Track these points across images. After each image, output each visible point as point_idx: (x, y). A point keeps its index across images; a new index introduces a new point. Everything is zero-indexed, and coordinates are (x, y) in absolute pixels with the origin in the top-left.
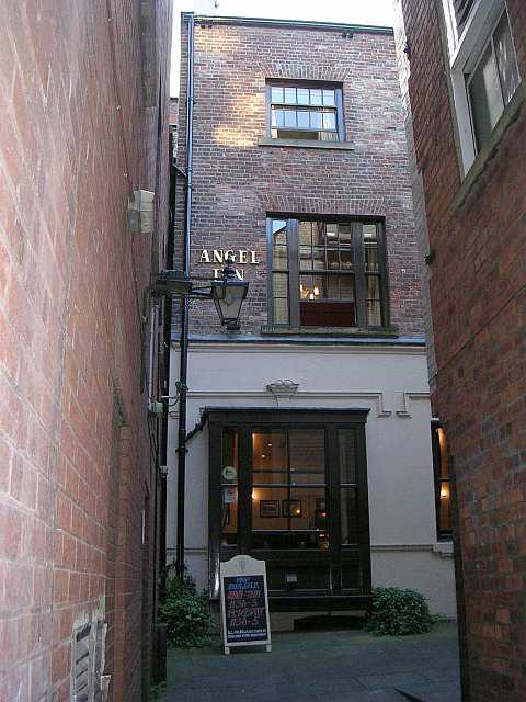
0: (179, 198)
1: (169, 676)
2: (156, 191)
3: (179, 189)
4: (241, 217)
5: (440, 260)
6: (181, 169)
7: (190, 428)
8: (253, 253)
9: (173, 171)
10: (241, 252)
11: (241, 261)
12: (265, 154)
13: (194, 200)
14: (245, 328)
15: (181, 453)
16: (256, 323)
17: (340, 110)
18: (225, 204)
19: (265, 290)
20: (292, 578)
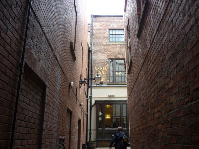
0: (90, 56)
3: (90, 54)
6: (91, 50)
8: (106, 67)
10: (103, 67)
11: (103, 69)
14: (104, 83)
15: (91, 110)
16: (106, 82)
18: (100, 57)
19: (108, 76)
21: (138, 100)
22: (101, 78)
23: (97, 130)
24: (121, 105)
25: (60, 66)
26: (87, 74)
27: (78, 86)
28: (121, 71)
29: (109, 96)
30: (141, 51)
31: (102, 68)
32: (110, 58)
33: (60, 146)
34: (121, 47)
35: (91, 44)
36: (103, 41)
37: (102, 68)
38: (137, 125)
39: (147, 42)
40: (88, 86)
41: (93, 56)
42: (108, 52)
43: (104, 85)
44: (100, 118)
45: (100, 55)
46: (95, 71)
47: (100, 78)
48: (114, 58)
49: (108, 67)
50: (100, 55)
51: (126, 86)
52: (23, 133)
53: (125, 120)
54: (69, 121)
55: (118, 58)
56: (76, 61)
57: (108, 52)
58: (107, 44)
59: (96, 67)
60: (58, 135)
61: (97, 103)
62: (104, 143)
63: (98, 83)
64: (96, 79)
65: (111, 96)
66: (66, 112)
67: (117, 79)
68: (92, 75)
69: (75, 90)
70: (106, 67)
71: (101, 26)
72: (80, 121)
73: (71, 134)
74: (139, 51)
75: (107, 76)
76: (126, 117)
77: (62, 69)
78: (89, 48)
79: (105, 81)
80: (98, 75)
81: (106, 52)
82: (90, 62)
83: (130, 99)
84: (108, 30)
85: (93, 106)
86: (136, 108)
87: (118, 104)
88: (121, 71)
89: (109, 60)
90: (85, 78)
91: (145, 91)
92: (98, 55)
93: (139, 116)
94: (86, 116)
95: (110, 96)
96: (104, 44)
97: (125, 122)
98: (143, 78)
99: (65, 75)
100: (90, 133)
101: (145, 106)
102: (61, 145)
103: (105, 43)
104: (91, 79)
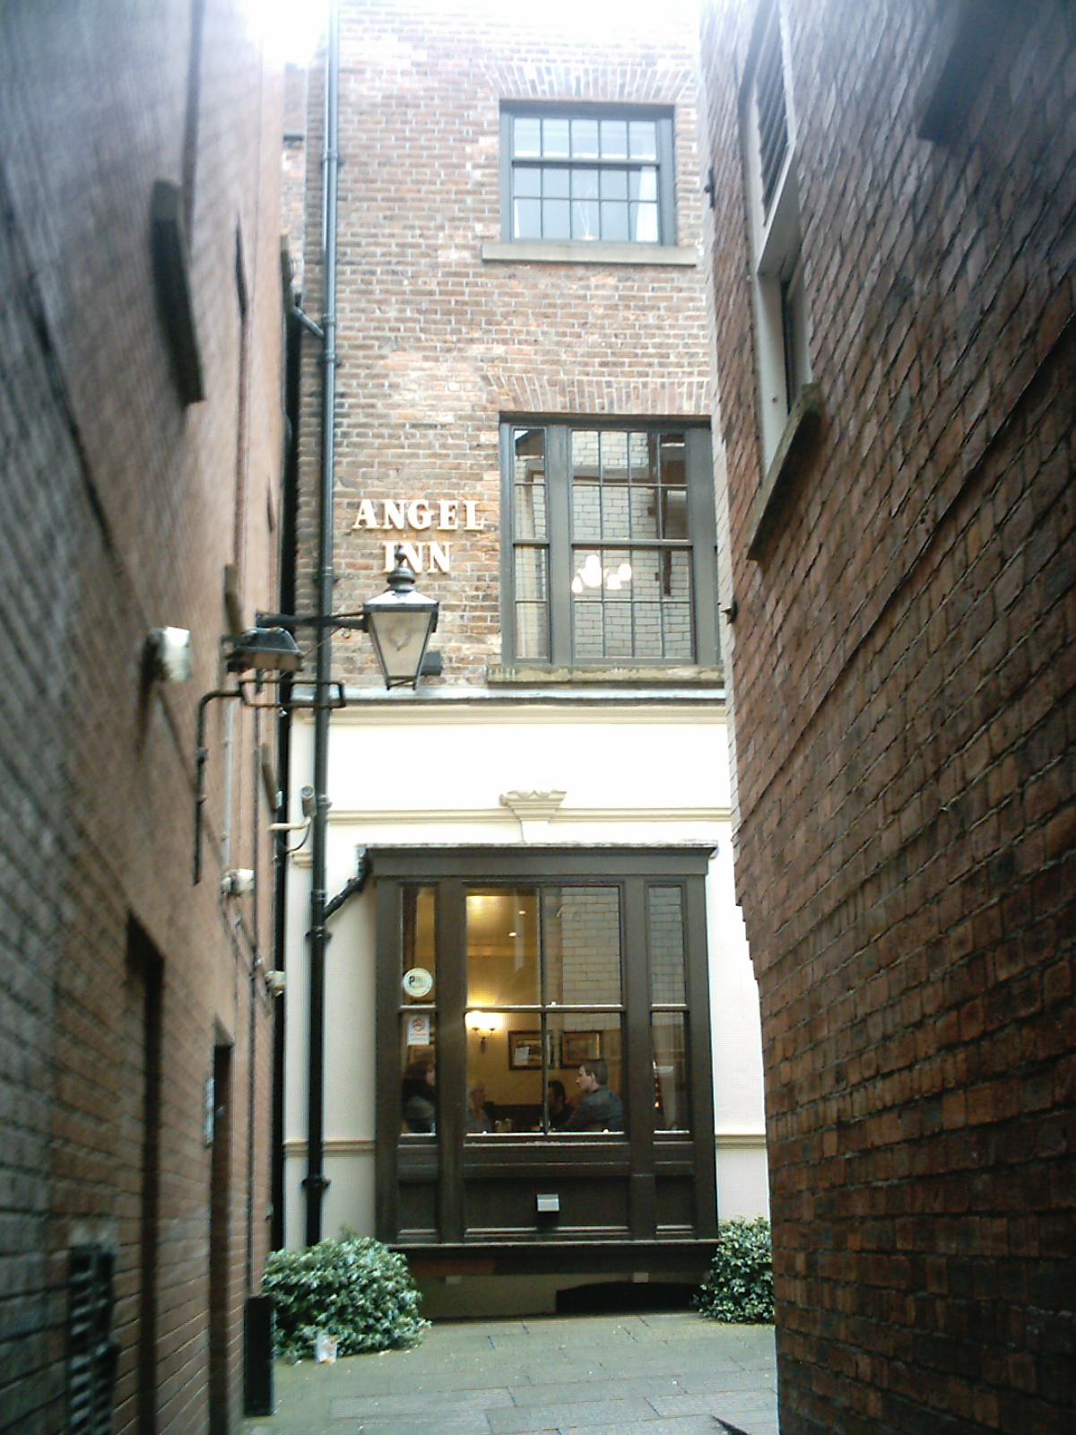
0: (308, 385)
1: (279, 1399)
2: (255, 868)
3: (307, 365)
4: (443, 426)
5: (742, 615)
6: (311, 319)
7: (335, 885)
8: (471, 505)
9: (295, 333)
10: (445, 504)
11: (445, 525)
12: (493, 281)
13: (341, 389)
14: (454, 670)
15: (317, 943)
16: (477, 660)
17: (666, 169)
18: (409, 396)
19: (497, 590)
20: (549, 1203)
21: (910, 820)
22: (433, 612)
23: (383, 1146)
24: (635, 889)
25: (74, 432)
26: (277, 569)
27: (212, 687)
28: (601, 547)
29: (505, 803)
30: (990, 267)
31: (427, 515)
32: (511, 407)
33: (78, 1329)
34: (621, 298)
35: (320, 260)
36: (442, 228)
37: (438, 507)
38: (885, 1091)
39: (1013, 194)
40: (286, 700)
41: (336, 385)
42: (499, 350)
43: (455, 684)
44: (417, 1024)
45: (414, 375)
46: (355, 540)
47: (421, 608)
48: (553, 403)
49: (495, 506)
51: (720, 701)
53: (664, 1046)
54: (135, 1055)
55: (595, 406)
56: (194, 409)
57: (499, 350)
58: (487, 262)
59: (366, 505)
60: (54, 1217)
61: (379, 869)
62: (453, 1280)
63: (405, 660)
64: (380, 621)
65: (523, 798)
66: (115, 954)
67: (587, 630)
68: (327, 583)
69: (187, 720)
71: (422, 70)
72: (223, 1055)
73: (164, 1203)
74: (947, 278)
75: (486, 597)
76: (680, 1019)
77: (85, 468)
78: (298, 297)
80: (396, 581)
81: (476, 350)
82: (307, 443)
83: (771, 825)
84: (493, 115)
85: (338, 903)
86: (875, 908)
87: (605, 882)
88: (601, 547)
89: (506, 427)
90: (264, 608)
91: (1037, 713)
92: (393, 379)
93: (929, 991)
94: (271, 1005)
95: (512, 808)
96: (453, 255)
97: (665, 1069)
98: (1014, 571)
99: (108, 544)
100: (315, 1188)
101: (1038, 875)
102: (82, 1319)
103: (466, 255)
104: (323, 623)
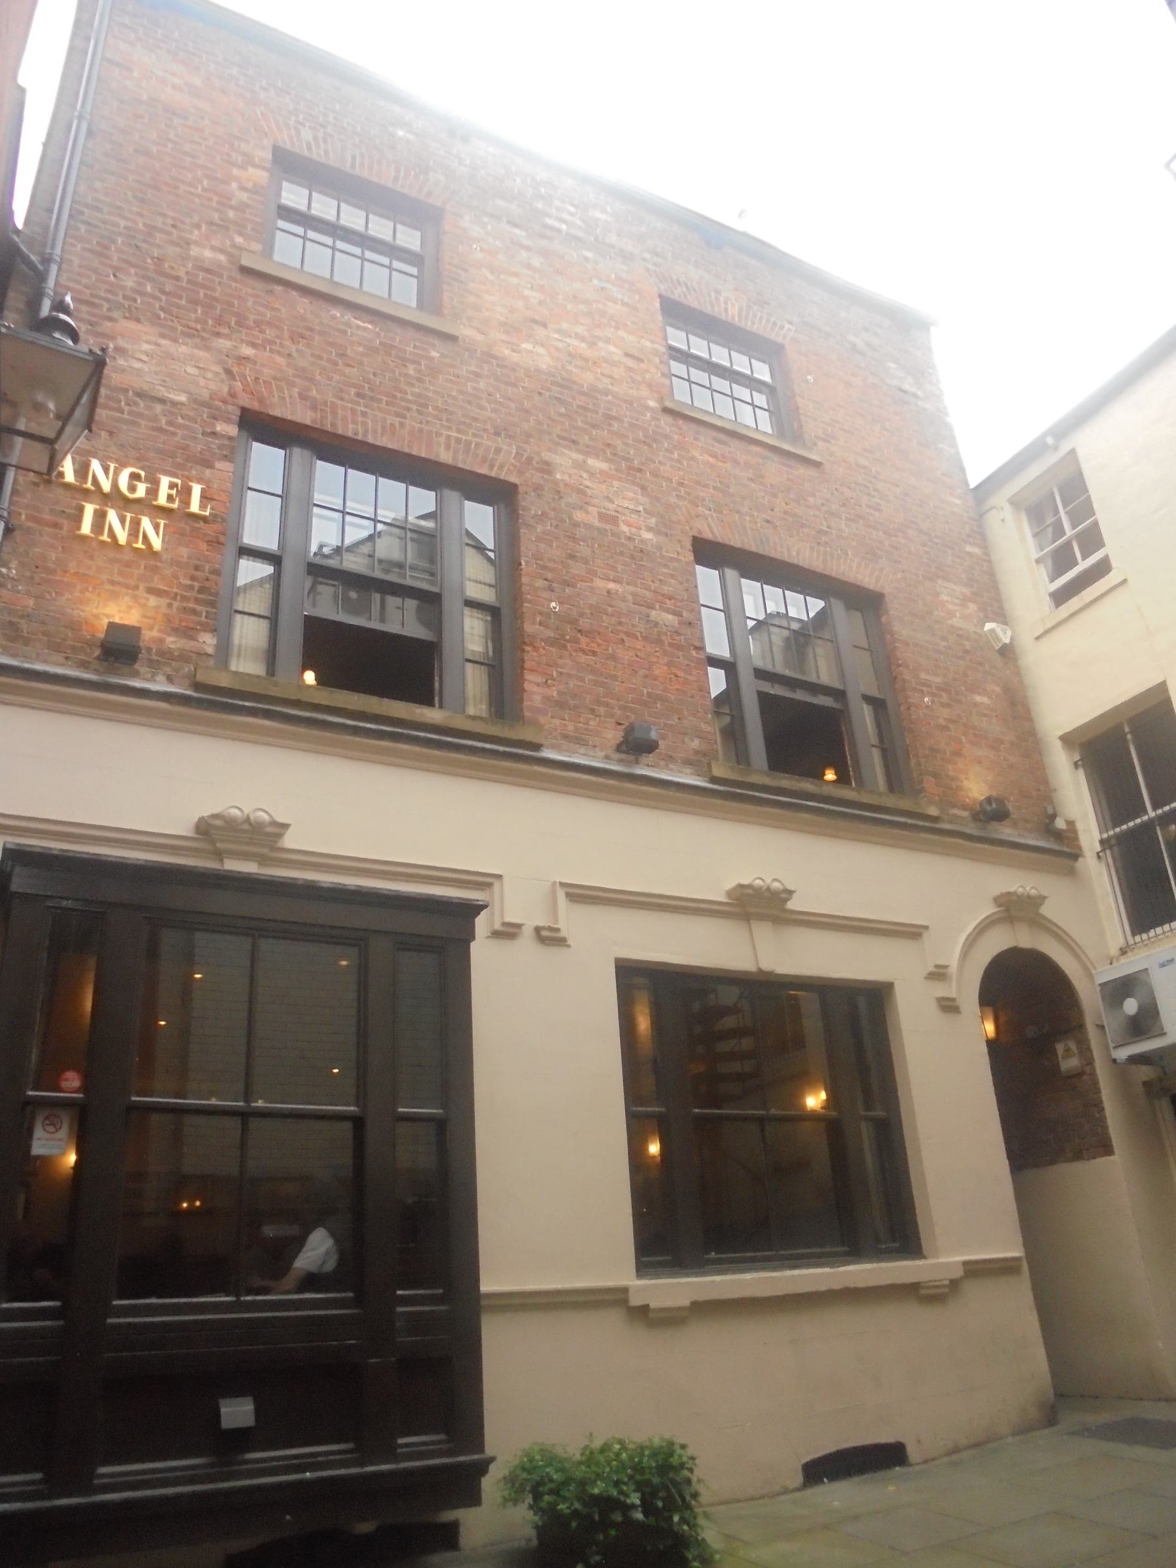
10: (165, 481)
11: (162, 500)
14: (151, 663)
42: (248, 351)
43: (152, 679)
45: (146, 347)
50: (146, 347)
52: (244, 1116)
70: (197, 489)
75: (202, 590)
79: (173, 642)
81: (224, 344)
92: (121, 342)
